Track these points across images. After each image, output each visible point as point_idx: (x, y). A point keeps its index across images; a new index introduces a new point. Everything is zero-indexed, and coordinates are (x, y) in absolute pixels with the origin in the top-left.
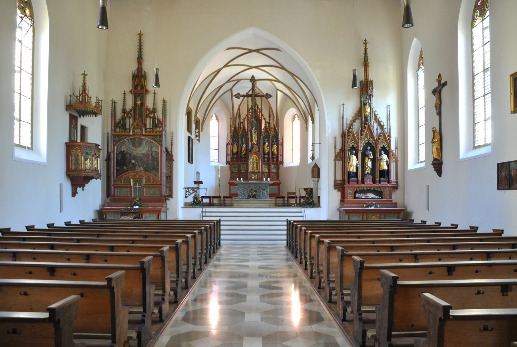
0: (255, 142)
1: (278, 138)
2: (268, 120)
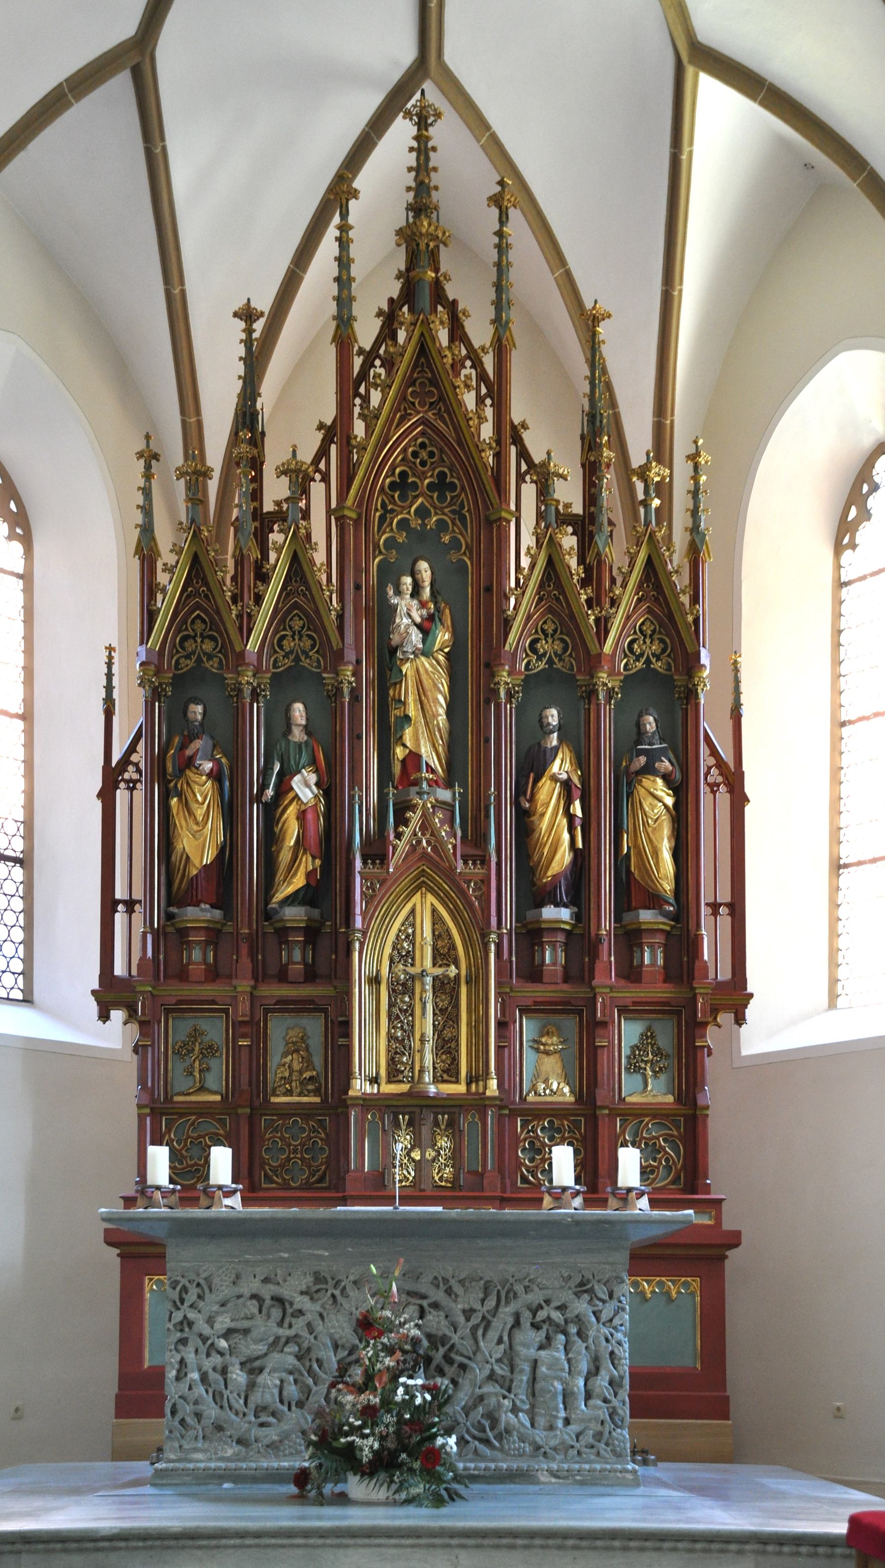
0: (424, 741)
1: (691, 695)
2: (569, 494)
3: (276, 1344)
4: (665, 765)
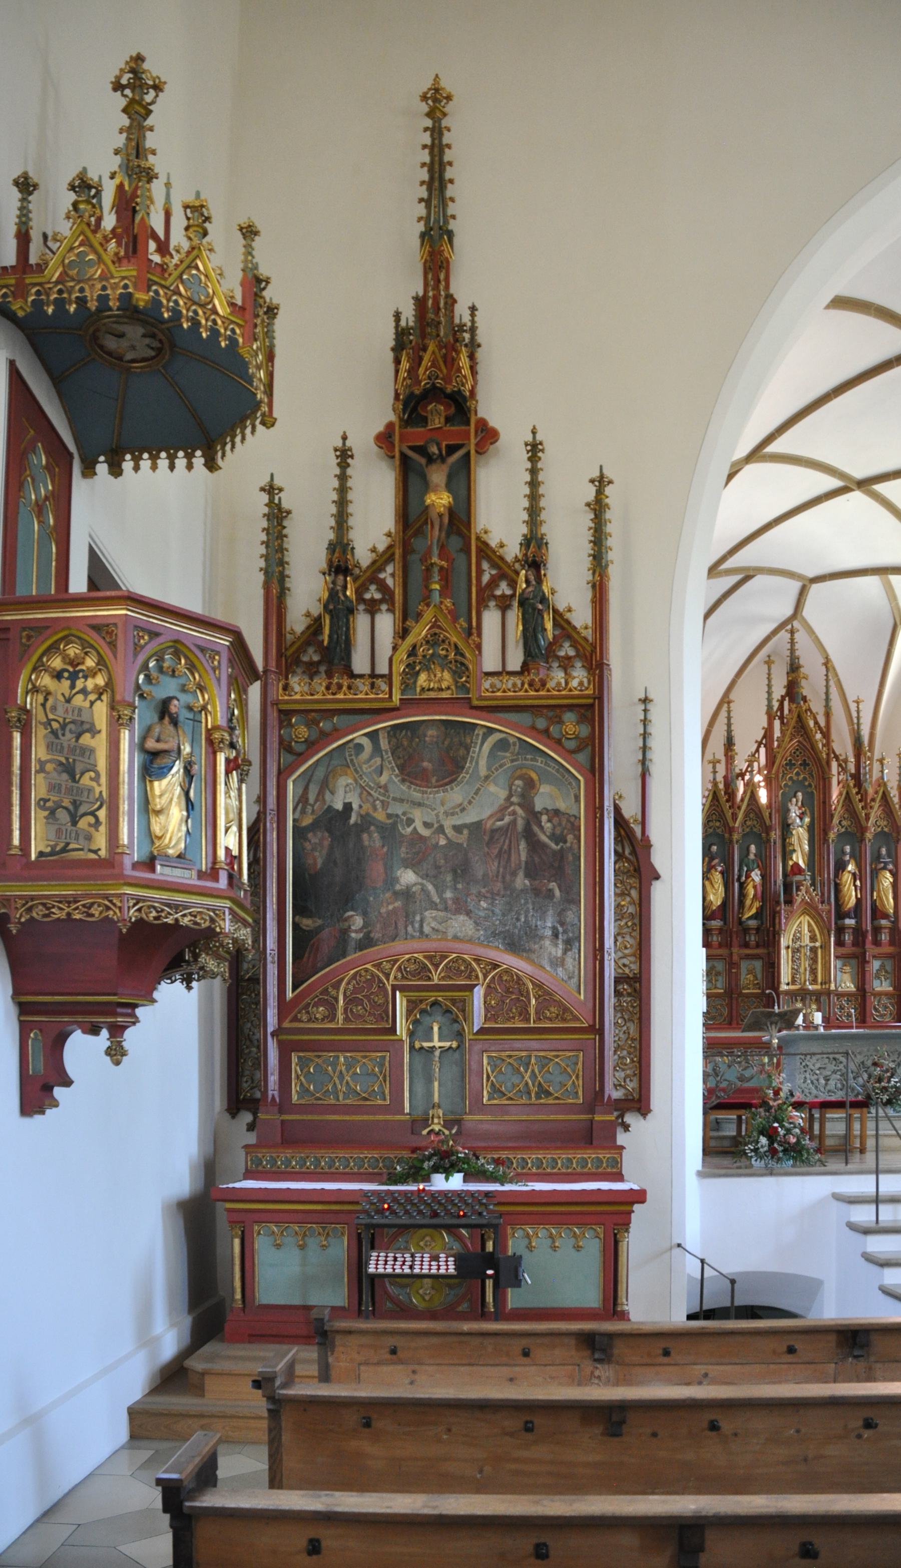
0: (799, 859)
3: (834, 1072)
4: (891, 867)
